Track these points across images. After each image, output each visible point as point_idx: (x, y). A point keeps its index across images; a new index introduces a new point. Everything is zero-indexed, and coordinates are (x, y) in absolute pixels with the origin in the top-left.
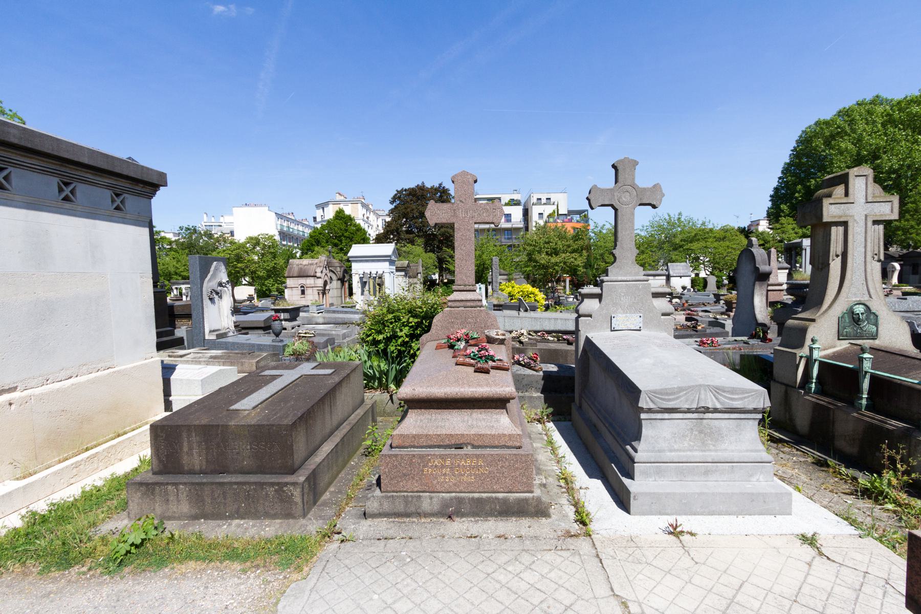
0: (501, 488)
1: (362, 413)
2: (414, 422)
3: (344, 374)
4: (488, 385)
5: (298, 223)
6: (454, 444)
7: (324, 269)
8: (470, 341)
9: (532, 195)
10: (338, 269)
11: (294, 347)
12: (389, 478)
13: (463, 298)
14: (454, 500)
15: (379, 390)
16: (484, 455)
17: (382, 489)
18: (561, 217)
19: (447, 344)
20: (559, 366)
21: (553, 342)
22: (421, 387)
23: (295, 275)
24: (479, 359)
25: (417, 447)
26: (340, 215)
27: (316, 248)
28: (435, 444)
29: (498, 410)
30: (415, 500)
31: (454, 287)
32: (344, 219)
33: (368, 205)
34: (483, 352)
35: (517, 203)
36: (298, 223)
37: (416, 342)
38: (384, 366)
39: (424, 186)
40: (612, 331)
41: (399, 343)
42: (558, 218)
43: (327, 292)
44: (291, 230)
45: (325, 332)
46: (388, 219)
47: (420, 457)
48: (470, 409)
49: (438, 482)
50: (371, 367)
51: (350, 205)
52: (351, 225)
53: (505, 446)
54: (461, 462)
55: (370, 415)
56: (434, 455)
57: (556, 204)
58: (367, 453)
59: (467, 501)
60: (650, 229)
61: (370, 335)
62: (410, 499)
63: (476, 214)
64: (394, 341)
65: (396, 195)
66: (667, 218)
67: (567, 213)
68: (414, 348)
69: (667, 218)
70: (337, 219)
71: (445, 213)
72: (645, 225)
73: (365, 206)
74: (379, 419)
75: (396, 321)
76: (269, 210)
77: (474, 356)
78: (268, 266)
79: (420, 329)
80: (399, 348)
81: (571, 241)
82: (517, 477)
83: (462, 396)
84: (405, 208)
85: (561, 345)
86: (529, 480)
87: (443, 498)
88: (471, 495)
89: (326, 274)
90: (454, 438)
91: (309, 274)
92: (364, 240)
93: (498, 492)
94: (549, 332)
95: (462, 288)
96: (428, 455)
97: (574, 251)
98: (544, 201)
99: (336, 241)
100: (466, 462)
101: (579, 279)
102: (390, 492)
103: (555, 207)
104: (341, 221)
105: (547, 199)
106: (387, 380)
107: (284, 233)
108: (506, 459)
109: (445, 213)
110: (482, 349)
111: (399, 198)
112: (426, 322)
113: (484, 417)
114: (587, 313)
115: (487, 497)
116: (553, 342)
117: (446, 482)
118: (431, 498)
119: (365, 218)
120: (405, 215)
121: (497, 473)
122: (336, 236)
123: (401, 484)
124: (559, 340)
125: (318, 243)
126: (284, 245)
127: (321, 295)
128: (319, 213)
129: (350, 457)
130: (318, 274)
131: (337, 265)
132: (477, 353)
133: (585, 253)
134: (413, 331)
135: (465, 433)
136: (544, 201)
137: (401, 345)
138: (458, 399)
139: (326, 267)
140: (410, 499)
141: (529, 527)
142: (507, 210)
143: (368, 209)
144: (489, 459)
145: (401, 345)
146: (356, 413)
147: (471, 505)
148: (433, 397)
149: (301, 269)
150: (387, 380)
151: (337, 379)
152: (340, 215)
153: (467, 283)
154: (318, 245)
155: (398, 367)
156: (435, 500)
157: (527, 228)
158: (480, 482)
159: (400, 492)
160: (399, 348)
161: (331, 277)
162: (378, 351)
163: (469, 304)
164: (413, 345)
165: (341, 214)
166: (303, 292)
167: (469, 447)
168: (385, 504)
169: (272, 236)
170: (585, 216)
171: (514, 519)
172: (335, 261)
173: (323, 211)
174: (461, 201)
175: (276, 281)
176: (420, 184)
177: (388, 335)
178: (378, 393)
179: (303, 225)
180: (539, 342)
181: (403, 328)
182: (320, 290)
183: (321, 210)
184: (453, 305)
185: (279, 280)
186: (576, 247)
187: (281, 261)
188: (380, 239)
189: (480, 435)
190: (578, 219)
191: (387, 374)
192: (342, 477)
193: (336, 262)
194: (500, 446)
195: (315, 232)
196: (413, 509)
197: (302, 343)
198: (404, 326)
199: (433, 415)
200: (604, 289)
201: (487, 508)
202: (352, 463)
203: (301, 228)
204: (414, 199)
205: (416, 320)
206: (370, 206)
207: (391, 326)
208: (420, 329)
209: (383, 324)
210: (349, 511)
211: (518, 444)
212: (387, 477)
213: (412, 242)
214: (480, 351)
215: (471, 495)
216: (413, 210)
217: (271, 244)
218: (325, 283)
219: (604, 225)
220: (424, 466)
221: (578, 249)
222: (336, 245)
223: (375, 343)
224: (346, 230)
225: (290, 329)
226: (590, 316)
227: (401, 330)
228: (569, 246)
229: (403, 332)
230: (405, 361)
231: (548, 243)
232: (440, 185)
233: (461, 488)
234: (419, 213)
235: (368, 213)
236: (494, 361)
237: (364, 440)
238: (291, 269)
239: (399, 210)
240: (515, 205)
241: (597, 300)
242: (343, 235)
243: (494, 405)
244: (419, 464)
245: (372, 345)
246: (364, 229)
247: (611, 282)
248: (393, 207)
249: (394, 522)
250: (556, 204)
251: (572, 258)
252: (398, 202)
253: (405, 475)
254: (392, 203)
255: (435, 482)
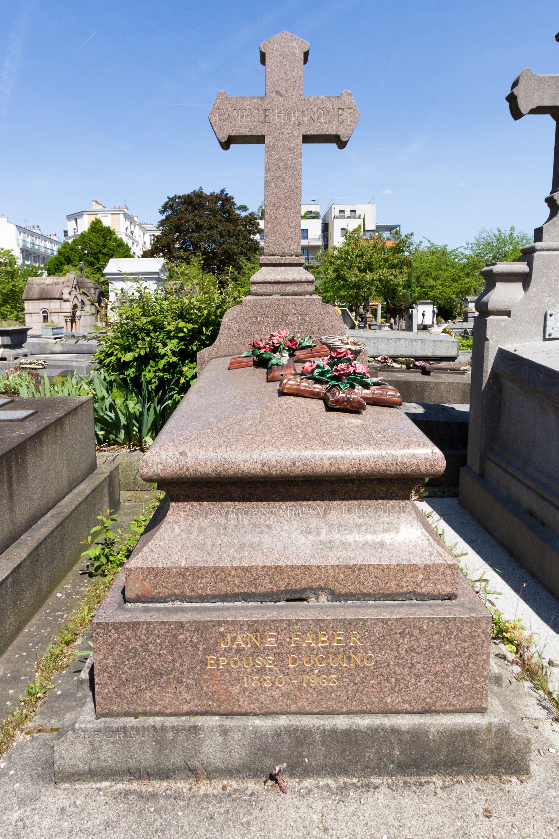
0: (405, 702)
1: (88, 492)
2: (184, 535)
3: (49, 418)
4: (369, 441)
5: (45, 238)
6: (286, 591)
7: (73, 289)
8: (297, 353)
9: (333, 206)
10: (92, 291)
11: (6, 382)
12: (116, 680)
13: (280, 278)
14: (286, 738)
15: (126, 446)
16: (365, 621)
17: (99, 709)
18: (368, 234)
19: (251, 359)
20: (424, 406)
21: (400, 370)
22: (201, 446)
23: (35, 297)
24: (333, 383)
25: (191, 599)
26: (96, 226)
27: (66, 267)
28: (236, 590)
29: (392, 503)
30: (182, 737)
31: (264, 259)
32: (102, 231)
33: (132, 217)
34: (341, 366)
35: (315, 216)
36: (45, 238)
37: (191, 365)
38: (134, 406)
39: (202, 193)
40: (545, 339)
41: (161, 367)
42: (364, 235)
43: (77, 318)
44: (37, 247)
45: (61, 363)
46: (158, 233)
47: (197, 629)
48: (323, 500)
49: (244, 690)
50: (112, 407)
51: (109, 215)
52: (110, 240)
53: (414, 593)
54: (304, 640)
55: (106, 491)
56: (234, 622)
57: (362, 217)
58: (92, 569)
59: (318, 737)
60: (476, 248)
61: (111, 354)
62: (170, 735)
63: (306, 119)
64: (152, 363)
65: (167, 203)
66: (497, 233)
67: (375, 228)
68: (187, 374)
69: (497, 233)
70: (92, 231)
71: (247, 116)
72: (470, 242)
73: (127, 217)
74: (124, 495)
75: (155, 330)
76: (8, 222)
77: (322, 374)
78: (4, 288)
79: (197, 342)
80: (161, 374)
81: (390, 254)
82: (447, 676)
83: (308, 470)
84: (179, 220)
85: (413, 375)
86: (477, 682)
87: (256, 731)
88: (328, 722)
89: (76, 297)
90: (285, 575)
91: (53, 296)
92: (126, 253)
93: (398, 712)
94: (394, 358)
95: (277, 259)
96: (219, 623)
97: (392, 267)
98: (348, 213)
99: (92, 259)
100: (317, 640)
101: (396, 303)
102: (118, 715)
103: (360, 221)
104: (98, 234)
105: (351, 211)
106: (140, 429)
107: (27, 251)
108: (421, 631)
109: (247, 116)
110: (339, 360)
111: (171, 207)
112: (207, 330)
113: (359, 521)
114: (502, 308)
115: (369, 728)
116: (400, 370)
117: (265, 690)
118: (225, 732)
119: (129, 233)
120: (178, 229)
121: (398, 664)
122: (92, 254)
123: (148, 694)
124: (408, 368)
125: (69, 261)
126: (27, 266)
127: (69, 323)
128: (70, 226)
129: (54, 583)
130: (66, 297)
131: (91, 285)
132: (327, 368)
133: (406, 270)
134: (184, 345)
135: (313, 562)
136: (348, 213)
137: (164, 370)
138: (296, 477)
139: (75, 288)
140: (170, 735)
141: (488, 814)
142: (305, 224)
143: (132, 222)
144: (378, 630)
145: (164, 370)
146: (76, 491)
147: (328, 749)
148: (231, 472)
149: (43, 289)
150: (140, 429)
151: (32, 428)
152: (96, 226)
153: (286, 250)
154: (68, 264)
155: (158, 409)
156: (236, 735)
157: (326, 246)
158: (352, 687)
159: (145, 714)
160: (161, 374)
161: (82, 301)
162: (124, 380)
163: (290, 288)
164: (185, 369)
165: (97, 226)
166: (46, 319)
167: (323, 598)
168: (105, 747)
169: (9, 252)
170: (396, 232)
171: (438, 780)
172: (87, 280)
173: (76, 223)
174: (278, 93)
175: (15, 307)
176: (197, 190)
177: (142, 353)
178: (125, 451)
179: (52, 241)
180: (380, 371)
181: (167, 341)
182: (69, 316)
183: (74, 222)
184: (260, 291)
185: (19, 307)
186: (396, 261)
187: (19, 282)
188: (146, 255)
189: (352, 568)
190: (388, 235)
191: (139, 418)
192: (30, 635)
193: (89, 283)
194: (402, 594)
195: (66, 248)
196: (177, 759)
197: (20, 376)
198: (170, 338)
199: (231, 516)
200: (535, 264)
201: (370, 754)
202: (59, 595)
203: (49, 245)
204: (190, 208)
205: (190, 326)
206: (135, 218)
207: (148, 339)
208: (197, 342)
209: (135, 336)
210: (22, 746)
211: (448, 590)
212: (110, 678)
213: (187, 261)
214: (336, 364)
215: (328, 722)
216: (188, 221)
217: (7, 261)
218: (75, 306)
219: (421, 242)
220: (207, 651)
221: (398, 264)
222: (91, 264)
223: (121, 366)
224: (105, 246)
225: (12, 359)
226: (508, 313)
227: (165, 345)
228: (386, 260)
229: (168, 348)
230: (171, 397)
231: (361, 256)
232: (223, 191)
233: (303, 703)
234: (195, 225)
235: (133, 226)
236: (366, 386)
237: (87, 547)
238: (30, 289)
239: (171, 222)
240: (313, 218)
241: (519, 285)
242: (100, 251)
243: (384, 489)
244: (195, 646)
245: (114, 370)
246: (127, 245)
247: (548, 250)
248: (163, 217)
249: (127, 793)
250: (362, 217)
251: (392, 274)
252: (170, 212)
253: (156, 673)
254: (162, 212)
255: (235, 690)
